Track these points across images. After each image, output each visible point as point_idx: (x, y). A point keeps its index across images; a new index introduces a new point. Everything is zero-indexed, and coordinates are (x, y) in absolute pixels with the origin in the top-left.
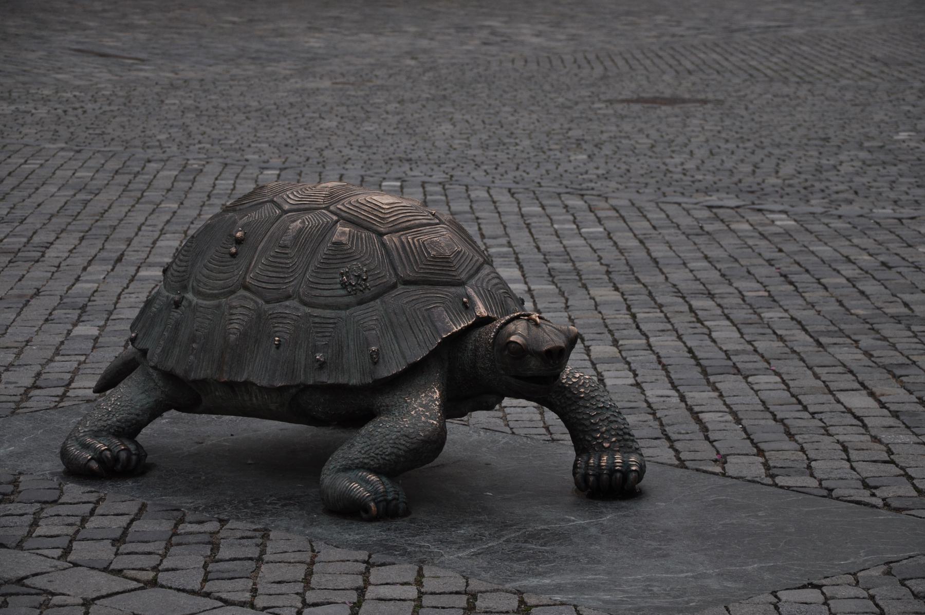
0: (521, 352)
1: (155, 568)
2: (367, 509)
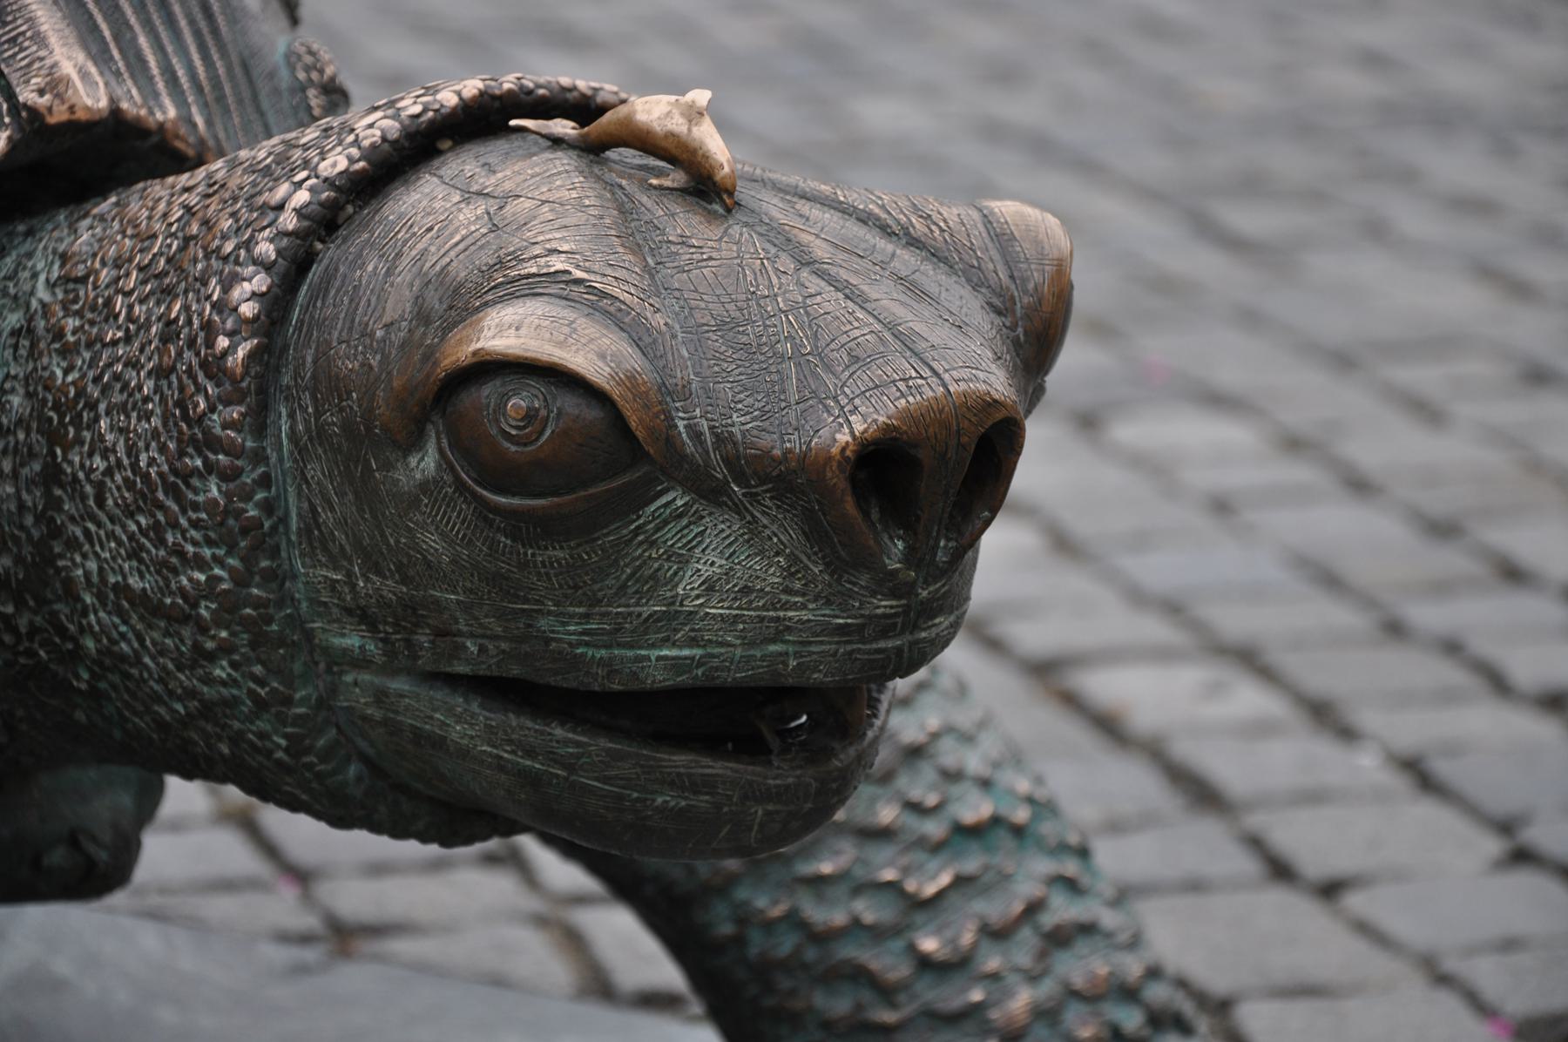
0: (597, 463)
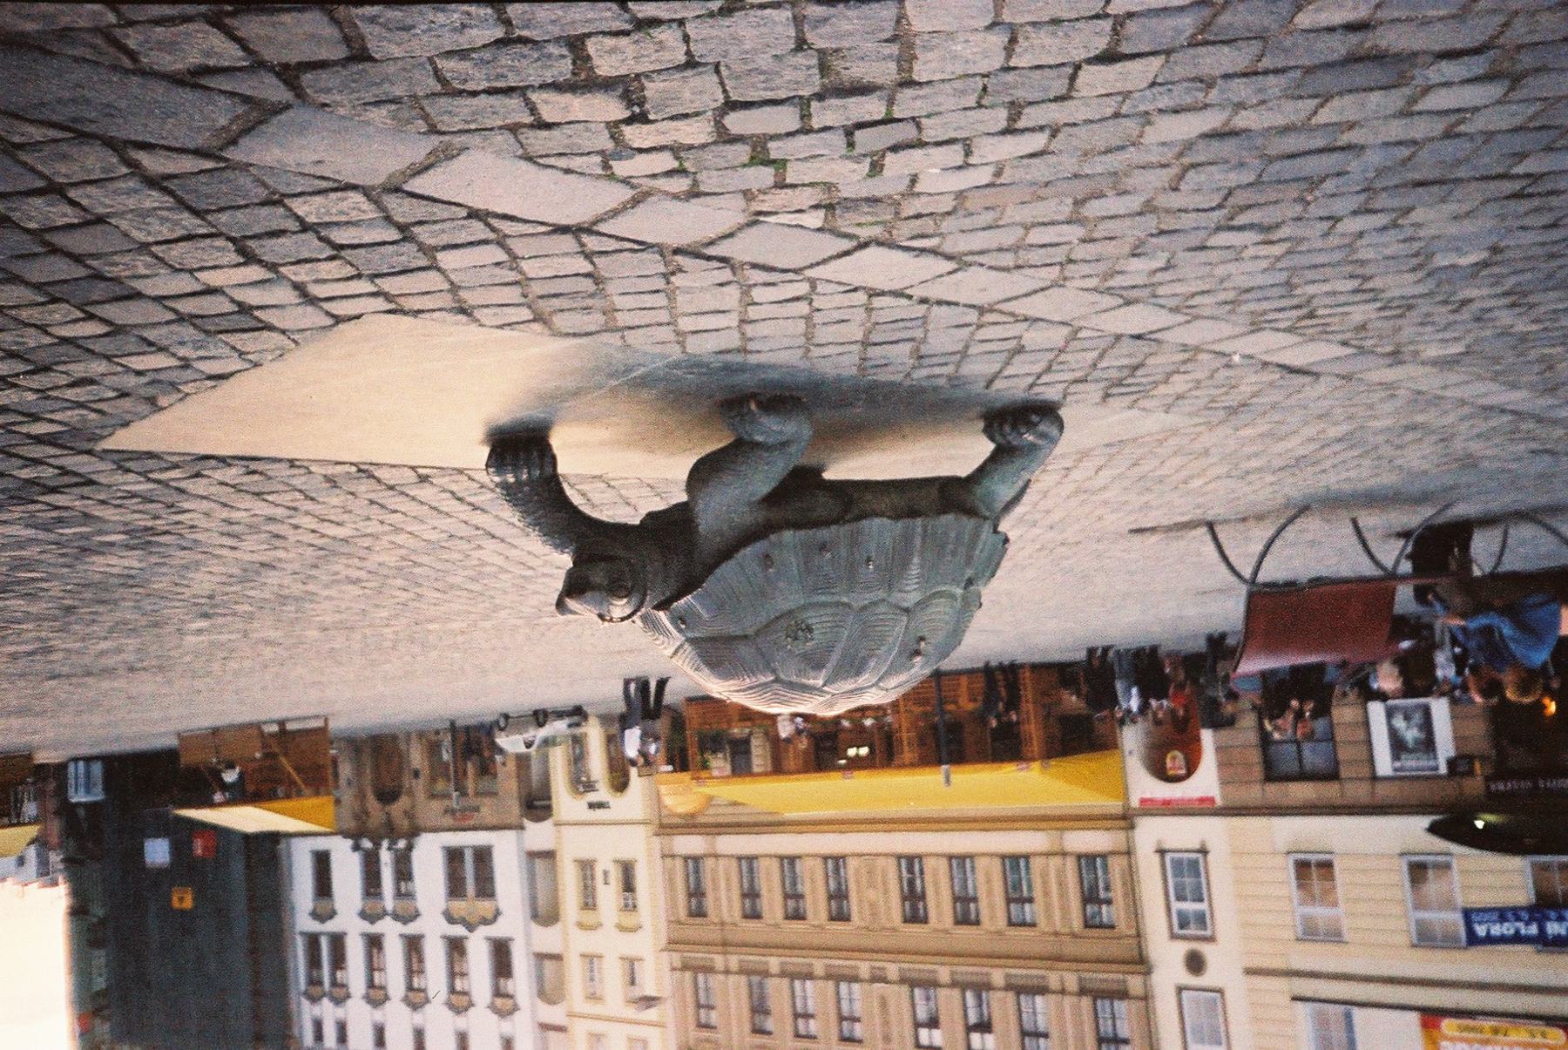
1: (980, 326)
2: (760, 405)
